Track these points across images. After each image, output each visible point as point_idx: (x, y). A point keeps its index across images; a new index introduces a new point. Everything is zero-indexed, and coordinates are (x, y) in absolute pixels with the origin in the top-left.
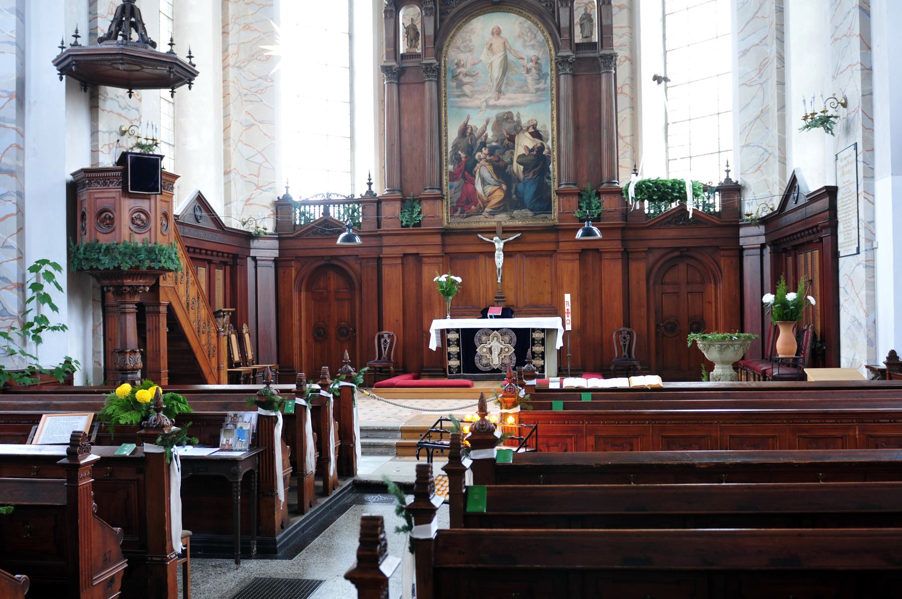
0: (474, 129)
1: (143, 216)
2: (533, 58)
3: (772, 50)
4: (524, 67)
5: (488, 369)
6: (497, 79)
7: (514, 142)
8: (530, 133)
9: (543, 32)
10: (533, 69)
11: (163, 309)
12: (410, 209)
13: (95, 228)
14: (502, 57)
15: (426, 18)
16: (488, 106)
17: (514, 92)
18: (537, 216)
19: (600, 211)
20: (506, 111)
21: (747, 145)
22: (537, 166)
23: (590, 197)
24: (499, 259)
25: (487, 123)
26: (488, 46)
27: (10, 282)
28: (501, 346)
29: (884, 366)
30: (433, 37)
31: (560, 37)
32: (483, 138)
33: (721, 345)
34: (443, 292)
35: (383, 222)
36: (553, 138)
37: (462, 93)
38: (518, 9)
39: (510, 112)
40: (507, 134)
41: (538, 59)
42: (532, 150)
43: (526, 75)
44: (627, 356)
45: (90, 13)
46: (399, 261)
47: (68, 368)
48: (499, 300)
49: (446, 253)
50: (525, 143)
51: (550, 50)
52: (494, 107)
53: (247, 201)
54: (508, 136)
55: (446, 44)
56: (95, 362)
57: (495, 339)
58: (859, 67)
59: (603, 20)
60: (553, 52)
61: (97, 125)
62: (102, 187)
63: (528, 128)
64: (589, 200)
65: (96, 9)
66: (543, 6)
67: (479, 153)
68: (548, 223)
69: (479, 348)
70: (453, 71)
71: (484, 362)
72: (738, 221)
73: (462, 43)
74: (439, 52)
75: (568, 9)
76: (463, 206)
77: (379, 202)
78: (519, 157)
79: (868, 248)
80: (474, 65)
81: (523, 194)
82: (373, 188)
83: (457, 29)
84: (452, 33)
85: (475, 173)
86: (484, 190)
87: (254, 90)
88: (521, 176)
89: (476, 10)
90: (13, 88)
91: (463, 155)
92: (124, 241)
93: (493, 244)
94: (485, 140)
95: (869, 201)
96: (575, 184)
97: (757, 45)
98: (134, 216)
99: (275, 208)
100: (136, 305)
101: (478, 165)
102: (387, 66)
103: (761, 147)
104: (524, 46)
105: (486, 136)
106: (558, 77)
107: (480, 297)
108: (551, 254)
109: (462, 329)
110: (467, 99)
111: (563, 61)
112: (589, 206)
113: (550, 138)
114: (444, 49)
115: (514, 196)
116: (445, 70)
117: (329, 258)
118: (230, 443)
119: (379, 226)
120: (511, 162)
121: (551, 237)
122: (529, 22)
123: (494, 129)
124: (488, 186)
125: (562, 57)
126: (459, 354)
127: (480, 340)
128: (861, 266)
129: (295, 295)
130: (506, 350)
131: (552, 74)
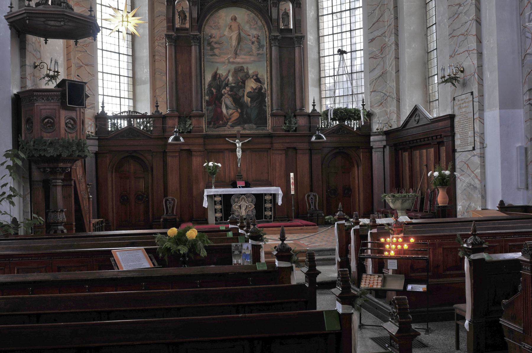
1: (72, 122)
2: (255, 36)
4: (250, 40)
6: (234, 47)
7: (245, 84)
8: (254, 79)
9: (261, 21)
10: (256, 42)
12: (184, 122)
13: (41, 129)
14: (238, 33)
15: (193, 7)
16: (229, 62)
17: (245, 55)
18: (259, 128)
19: (297, 125)
20: (240, 65)
23: (290, 117)
24: (239, 154)
25: (229, 72)
26: (229, 26)
30: (197, 19)
31: (272, 25)
32: (226, 80)
33: (403, 200)
36: (267, 83)
37: (213, 54)
38: (247, 6)
39: (243, 66)
41: (259, 36)
42: (256, 89)
44: (314, 208)
46: (177, 154)
48: (240, 177)
49: (206, 150)
50: (251, 85)
51: (266, 32)
52: (233, 63)
54: (241, 81)
56: (25, 218)
57: (243, 200)
58: (475, 52)
60: (267, 33)
62: (46, 102)
63: (253, 76)
64: (290, 119)
66: (262, 6)
67: (224, 90)
68: (264, 132)
69: (233, 206)
72: (370, 133)
73: (213, 24)
74: (200, 29)
75: (277, 8)
77: (164, 117)
78: (248, 93)
79: (482, 147)
82: (316, 108)
83: (210, 15)
84: (208, 17)
86: (227, 112)
88: (249, 104)
91: (214, 91)
92: (62, 138)
93: (235, 145)
94: (228, 82)
95: (481, 122)
96: (281, 110)
97: (380, 36)
98: (67, 121)
99: (95, 120)
100: (62, 180)
101: (224, 97)
102: (169, 35)
103: (382, 92)
104: (250, 28)
105: (228, 80)
107: (226, 176)
108: (267, 150)
109: (223, 194)
110: (217, 57)
111: (274, 38)
112: (290, 122)
113: (266, 83)
114: (203, 27)
115: (245, 116)
117: (131, 152)
118: (239, 263)
121: (268, 140)
122: (253, 14)
124: (229, 110)
125: (274, 36)
126: (221, 209)
127: (234, 201)
129: (109, 175)
130: (250, 206)
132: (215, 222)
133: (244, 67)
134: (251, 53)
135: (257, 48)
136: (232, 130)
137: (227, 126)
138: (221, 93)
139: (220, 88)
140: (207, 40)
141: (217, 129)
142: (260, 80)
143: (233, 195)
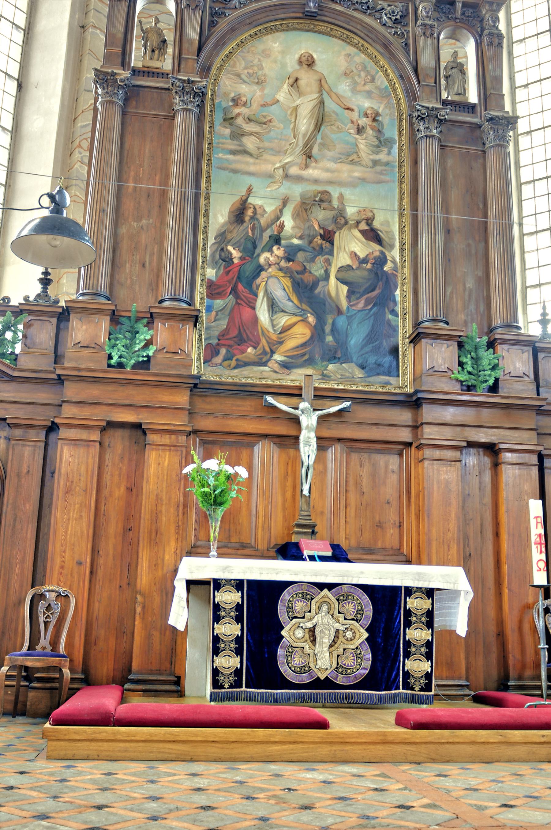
0: (259, 211)
2: (369, 112)
4: (352, 122)
5: (306, 679)
6: (305, 135)
7: (332, 243)
10: (368, 128)
12: (128, 335)
15: (187, 14)
16: (286, 176)
17: (335, 160)
20: (320, 188)
22: (373, 290)
23: (476, 348)
25: (285, 202)
26: (292, 80)
28: (337, 626)
32: (275, 228)
34: (205, 495)
36: (402, 244)
37: (239, 148)
40: (320, 227)
41: (377, 114)
42: (364, 261)
43: (357, 136)
51: (399, 104)
52: (299, 179)
54: (322, 232)
57: (325, 608)
63: (358, 223)
67: (266, 255)
69: (287, 628)
70: (225, 110)
71: (297, 661)
73: (245, 68)
76: (230, 346)
80: (264, 105)
81: (347, 336)
85: (258, 289)
86: (272, 321)
88: (344, 304)
89: (276, 20)
91: (236, 254)
101: (263, 274)
104: (354, 90)
105: (282, 227)
106: (414, 143)
109: (249, 581)
110: (251, 160)
113: (397, 244)
115: (329, 339)
116: (213, 106)
119: (57, 358)
122: (363, 56)
123: (296, 216)
127: (290, 609)
130: (349, 634)
131: (400, 140)
132: (209, 689)
133: (332, 193)
134: (354, 157)
135: (374, 146)
136: (287, 377)
137: (270, 364)
138: (258, 261)
139: (255, 247)
140: (224, 109)
141: (236, 371)
142: (379, 235)
143: (288, 584)
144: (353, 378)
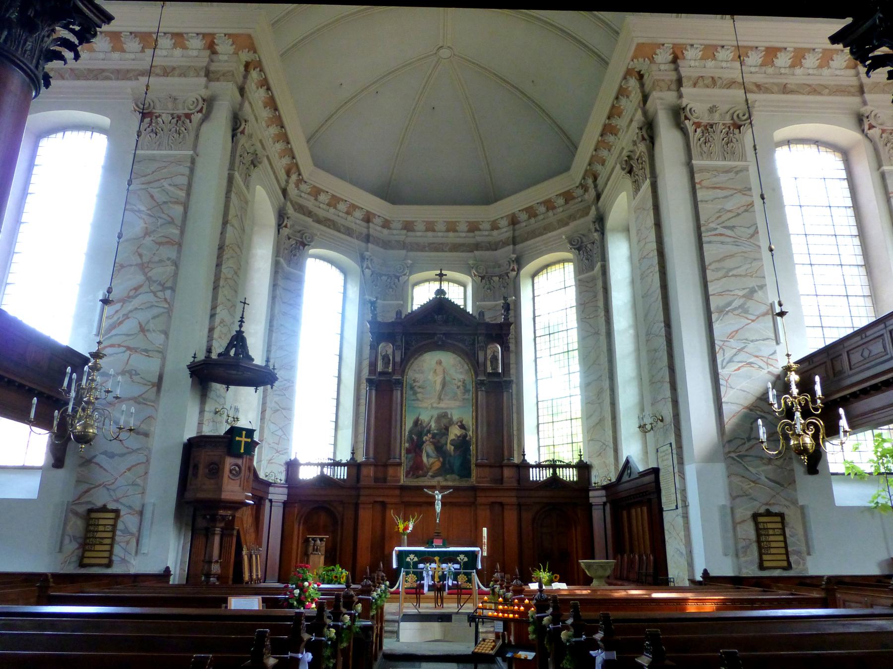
1: (237, 469)
3: (606, 385)
11: (235, 532)
16: (432, 408)
17: (449, 400)
20: (444, 411)
21: (592, 440)
24: (438, 507)
27: (134, 510)
29: (701, 579)
35: (362, 478)
36: (473, 429)
37: (415, 398)
41: (465, 380)
42: (460, 437)
45: (208, 337)
47: (167, 572)
51: (472, 375)
53: (270, 460)
55: (408, 367)
58: (670, 400)
59: (505, 360)
61: (204, 407)
65: (213, 334)
74: (403, 373)
78: (451, 440)
84: (411, 362)
86: (428, 461)
87: (281, 388)
90: (156, 380)
96: (486, 459)
101: (425, 445)
105: (431, 426)
113: (471, 429)
114: (406, 371)
120: (446, 444)
125: (480, 380)
128: (679, 516)
129: (296, 527)
144: (821, 75)
